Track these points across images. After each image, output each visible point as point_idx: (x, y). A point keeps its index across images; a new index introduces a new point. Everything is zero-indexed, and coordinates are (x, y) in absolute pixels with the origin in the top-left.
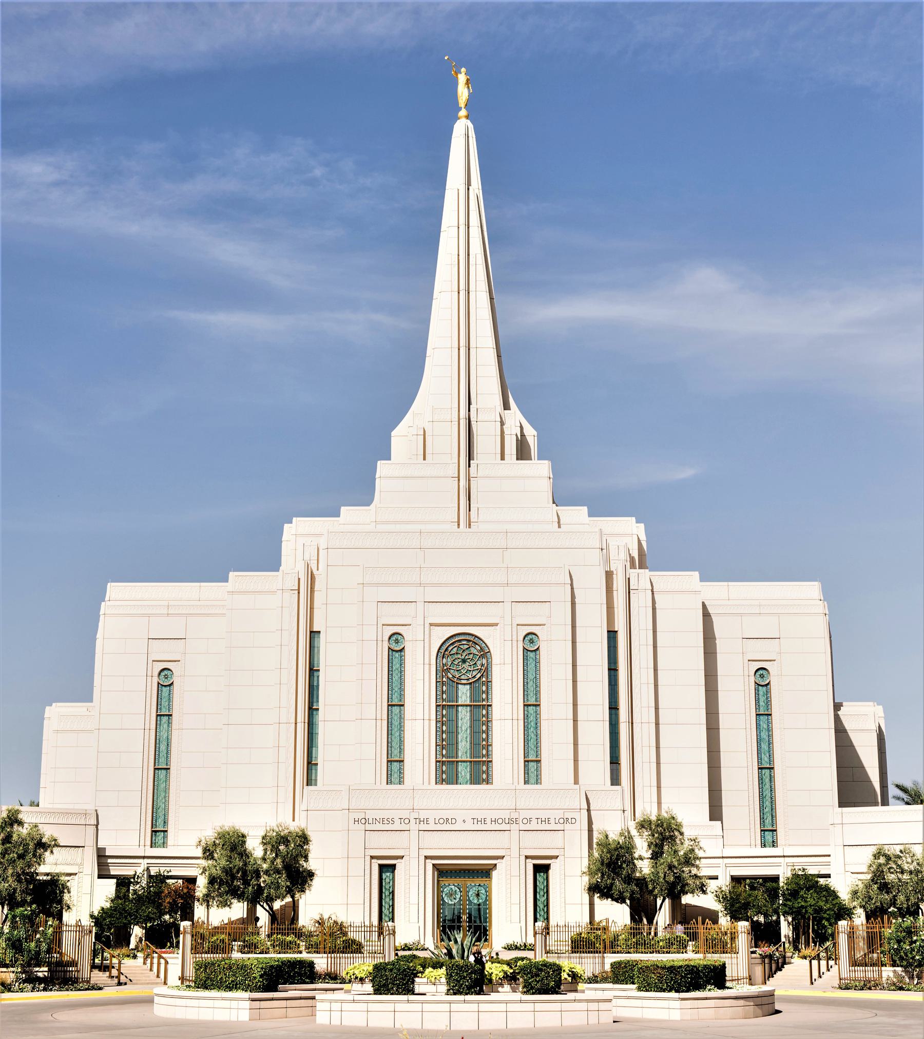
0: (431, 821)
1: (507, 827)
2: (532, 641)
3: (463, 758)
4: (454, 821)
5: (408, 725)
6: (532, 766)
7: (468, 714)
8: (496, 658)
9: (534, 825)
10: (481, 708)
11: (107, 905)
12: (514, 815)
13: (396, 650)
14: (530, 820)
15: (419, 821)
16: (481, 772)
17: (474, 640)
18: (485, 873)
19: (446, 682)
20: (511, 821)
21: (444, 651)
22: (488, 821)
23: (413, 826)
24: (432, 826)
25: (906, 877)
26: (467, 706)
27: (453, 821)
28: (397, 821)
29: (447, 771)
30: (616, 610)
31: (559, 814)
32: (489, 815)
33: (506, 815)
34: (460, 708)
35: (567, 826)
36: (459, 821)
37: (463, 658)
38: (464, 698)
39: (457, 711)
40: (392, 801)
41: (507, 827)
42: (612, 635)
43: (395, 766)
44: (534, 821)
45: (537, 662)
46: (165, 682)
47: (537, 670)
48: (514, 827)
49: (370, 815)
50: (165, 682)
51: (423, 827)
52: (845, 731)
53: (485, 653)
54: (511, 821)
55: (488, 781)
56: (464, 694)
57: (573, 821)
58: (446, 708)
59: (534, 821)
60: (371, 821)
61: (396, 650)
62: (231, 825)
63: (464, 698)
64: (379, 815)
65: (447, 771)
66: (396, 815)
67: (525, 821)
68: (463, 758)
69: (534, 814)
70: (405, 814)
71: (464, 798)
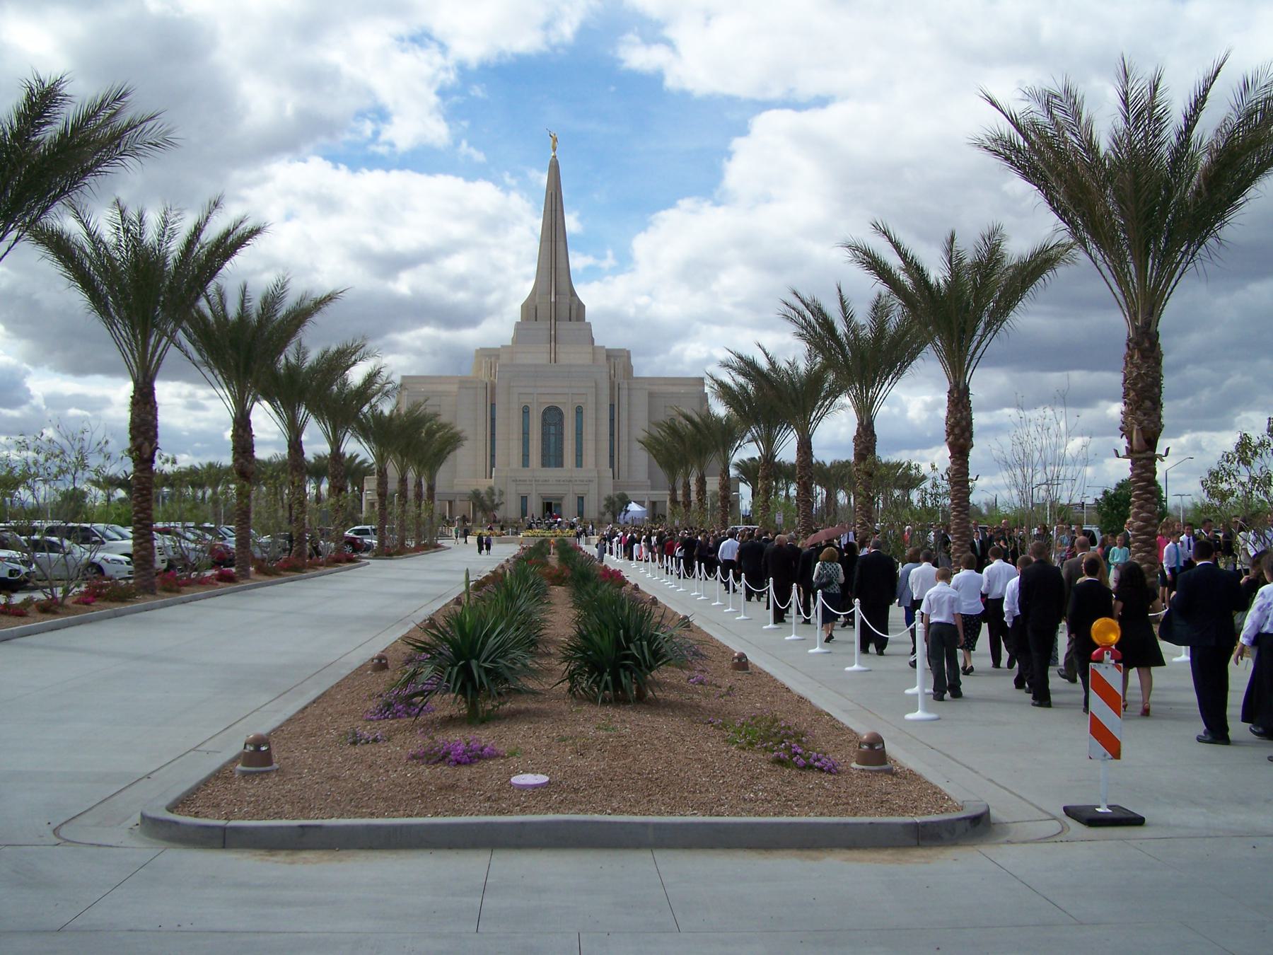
3: (552, 457)
6: (579, 463)
11: (365, 171)
13: (526, 411)
16: (560, 464)
17: (557, 409)
19: (545, 423)
21: (544, 413)
25: (356, 448)
37: (552, 417)
40: (526, 474)
42: (612, 406)
43: (525, 461)
52: (952, 447)
53: (561, 414)
56: (553, 430)
61: (526, 411)
68: (552, 457)
71: (552, 473)
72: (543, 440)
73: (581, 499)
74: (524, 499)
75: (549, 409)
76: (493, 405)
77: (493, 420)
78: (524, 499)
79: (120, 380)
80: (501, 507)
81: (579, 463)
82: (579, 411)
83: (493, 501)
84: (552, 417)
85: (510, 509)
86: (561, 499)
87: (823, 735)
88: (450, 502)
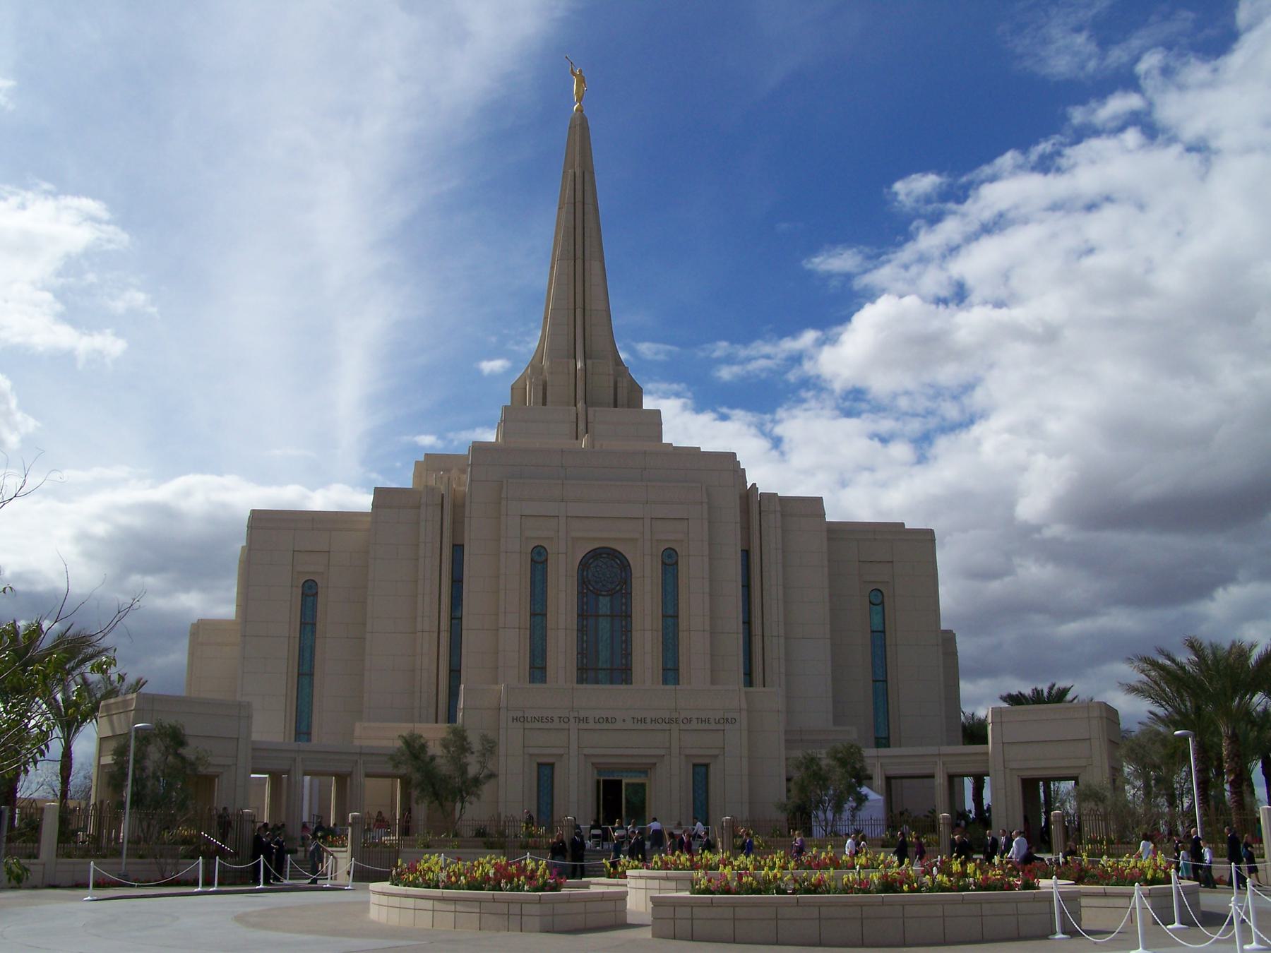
1: (720, 727)
2: (539, 554)
5: (636, 636)
6: (671, 672)
8: (636, 572)
9: (694, 725)
10: (624, 616)
12: (675, 715)
13: (539, 560)
15: (579, 720)
16: (622, 673)
17: (613, 554)
21: (584, 565)
22: (648, 721)
24: (591, 725)
27: (613, 720)
28: (591, 721)
29: (587, 671)
30: (739, 537)
35: (728, 726)
37: (604, 574)
41: (667, 727)
42: (746, 554)
43: (538, 669)
45: (545, 573)
46: (309, 592)
47: (545, 581)
48: (674, 726)
50: (309, 592)
51: (583, 726)
53: (625, 566)
54: (671, 721)
55: (581, 680)
58: (585, 615)
61: (539, 560)
62: (173, 722)
65: (587, 671)
68: (604, 661)
71: (601, 698)
72: (581, 630)
73: (701, 772)
74: (546, 772)
75: (596, 554)
76: (458, 549)
77: (457, 582)
78: (546, 772)
79: (634, 908)
80: (486, 789)
81: (671, 672)
82: (670, 562)
83: (463, 769)
84: (604, 574)
85: (510, 795)
86: (646, 770)
87: (772, 868)
88: (342, 779)
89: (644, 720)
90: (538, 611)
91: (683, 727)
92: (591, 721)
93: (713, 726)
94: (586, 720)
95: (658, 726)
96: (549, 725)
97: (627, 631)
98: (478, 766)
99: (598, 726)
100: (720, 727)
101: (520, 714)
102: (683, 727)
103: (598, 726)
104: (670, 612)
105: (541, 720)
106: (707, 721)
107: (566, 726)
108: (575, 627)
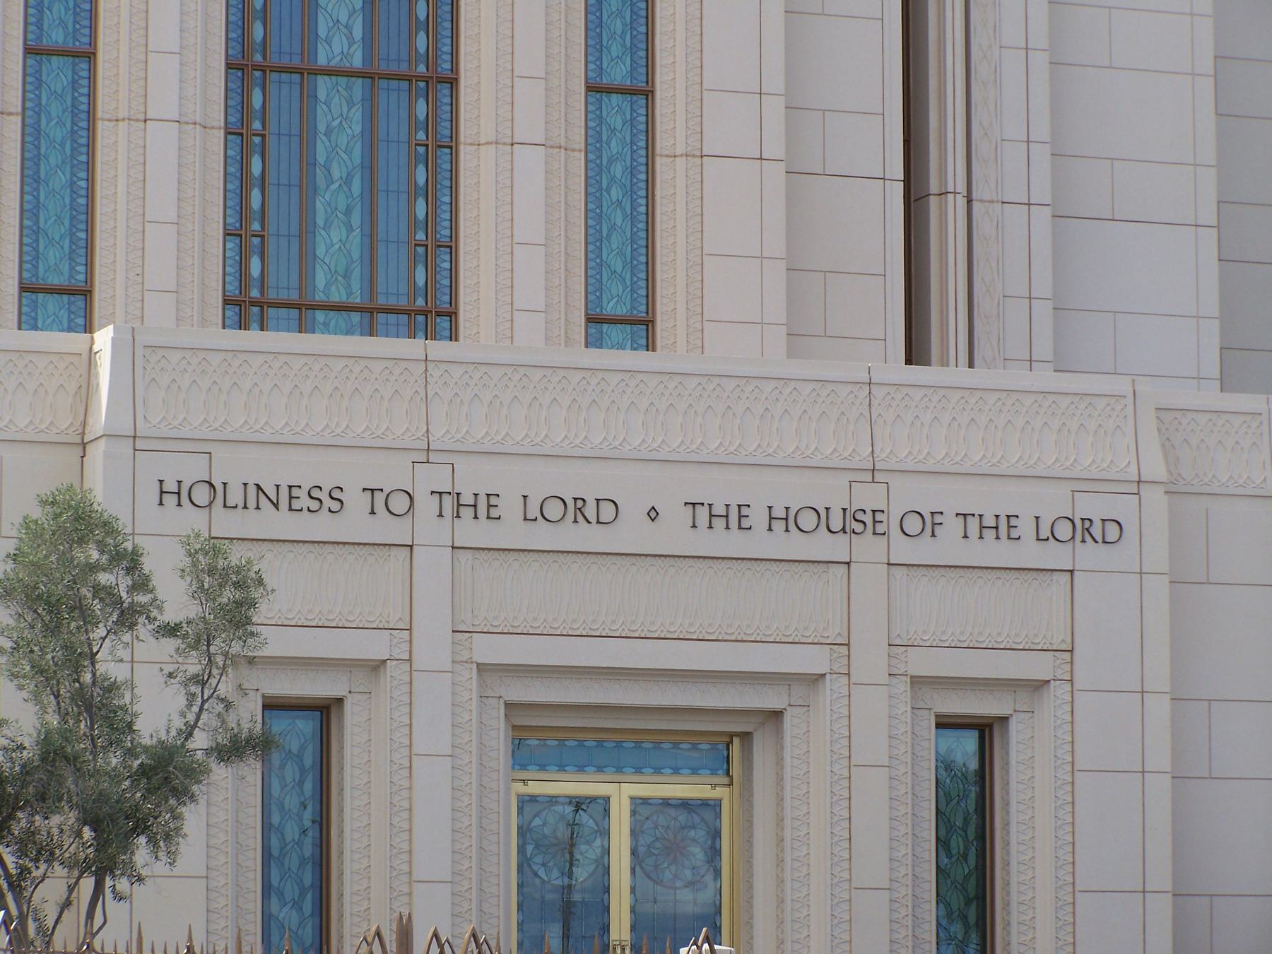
0: (509, 507)
1: (1056, 556)
4: (607, 512)
5: (478, 170)
6: (622, 313)
7: (357, 114)
9: (950, 545)
12: (869, 497)
14: (932, 523)
15: (455, 504)
18: (726, 742)
20: (860, 522)
22: (757, 518)
23: (429, 527)
24: (511, 532)
26: (350, 74)
28: (356, 501)
31: (1052, 503)
32: (762, 493)
33: (833, 494)
34: (323, 83)
35: (1089, 555)
36: (633, 511)
38: (339, 44)
39: (308, 100)
41: (835, 547)
44: (951, 526)
48: (867, 547)
49: (235, 469)
51: (471, 531)
54: (860, 522)
57: (607, 512)
59: (951, 526)
60: (235, 497)
63: (339, 44)
64: (273, 470)
66: (352, 474)
67: (913, 525)
69: (949, 498)
70: (392, 473)
71: (325, 395)
81: (622, 313)
89: (737, 517)
90: (56, 37)
91: (903, 550)
92: (356, 501)
93: (1029, 553)
94: (487, 507)
95: (796, 546)
96: (322, 526)
97: (439, 147)
98: (175, 699)
99: (543, 536)
100: (1056, 556)
101: (190, 470)
102: (903, 550)
103: (543, 536)
104: (618, 74)
105: (286, 498)
106: (1004, 528)
107: (396, 531)
108: (218, 117)
